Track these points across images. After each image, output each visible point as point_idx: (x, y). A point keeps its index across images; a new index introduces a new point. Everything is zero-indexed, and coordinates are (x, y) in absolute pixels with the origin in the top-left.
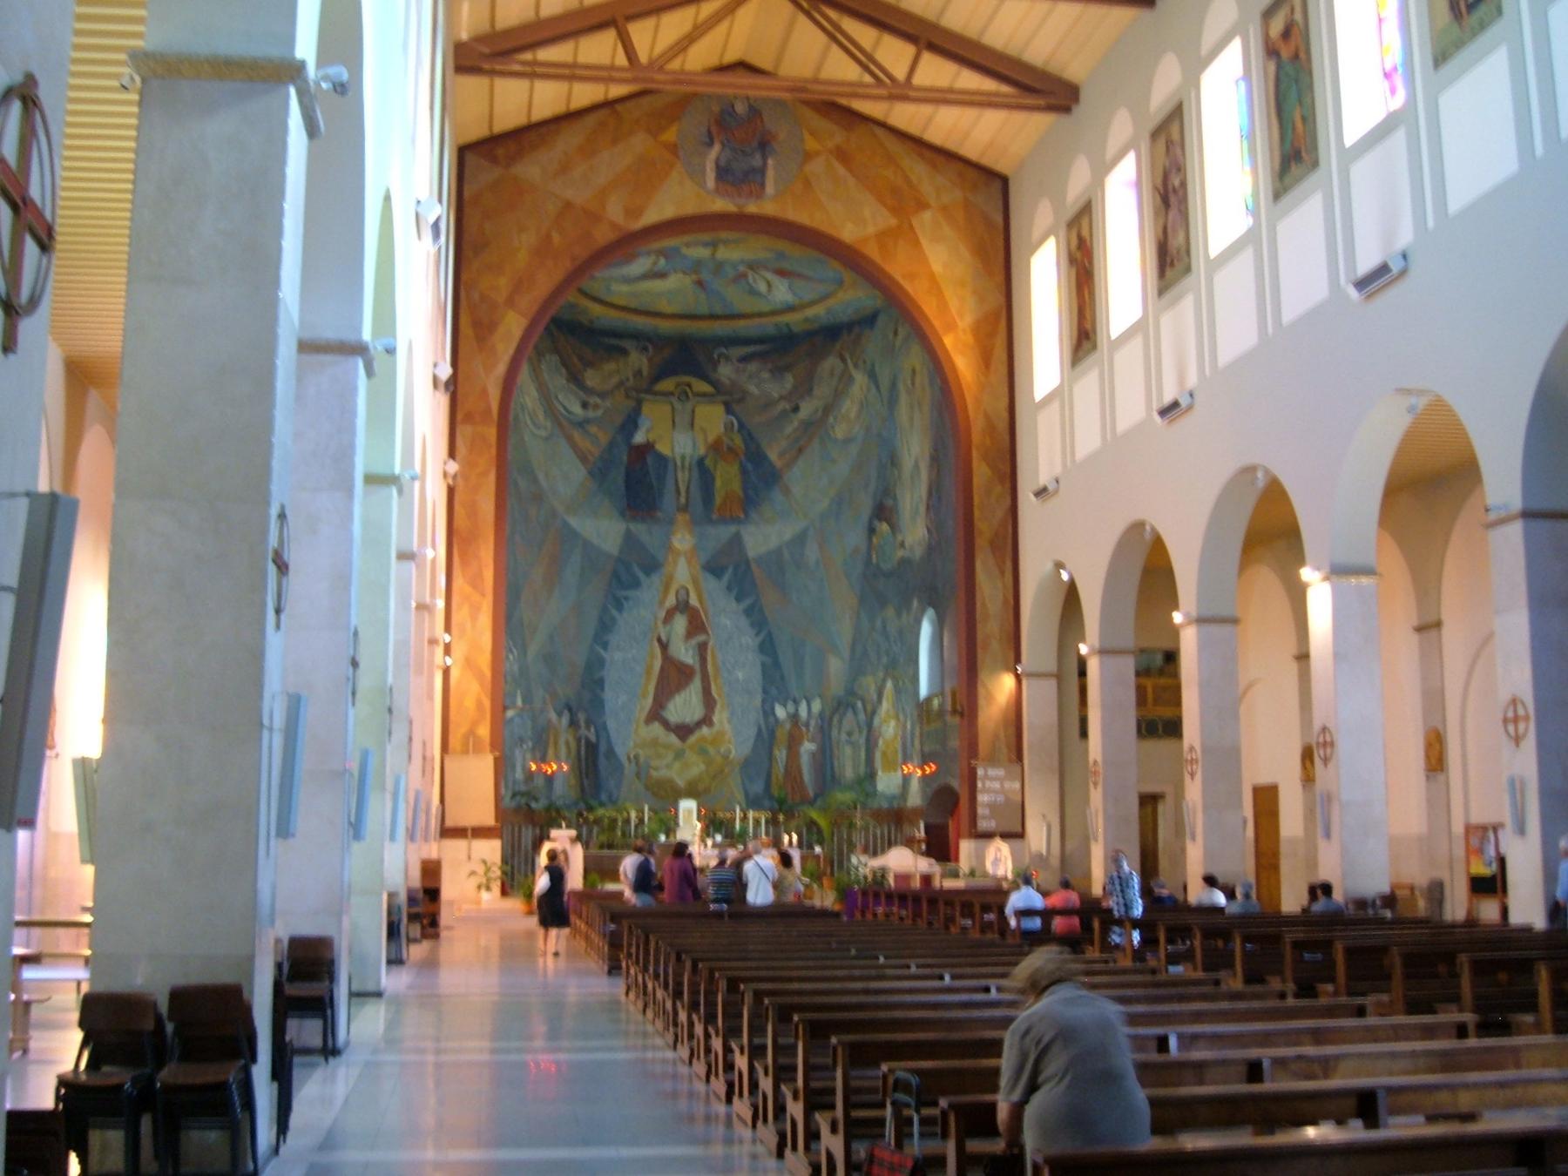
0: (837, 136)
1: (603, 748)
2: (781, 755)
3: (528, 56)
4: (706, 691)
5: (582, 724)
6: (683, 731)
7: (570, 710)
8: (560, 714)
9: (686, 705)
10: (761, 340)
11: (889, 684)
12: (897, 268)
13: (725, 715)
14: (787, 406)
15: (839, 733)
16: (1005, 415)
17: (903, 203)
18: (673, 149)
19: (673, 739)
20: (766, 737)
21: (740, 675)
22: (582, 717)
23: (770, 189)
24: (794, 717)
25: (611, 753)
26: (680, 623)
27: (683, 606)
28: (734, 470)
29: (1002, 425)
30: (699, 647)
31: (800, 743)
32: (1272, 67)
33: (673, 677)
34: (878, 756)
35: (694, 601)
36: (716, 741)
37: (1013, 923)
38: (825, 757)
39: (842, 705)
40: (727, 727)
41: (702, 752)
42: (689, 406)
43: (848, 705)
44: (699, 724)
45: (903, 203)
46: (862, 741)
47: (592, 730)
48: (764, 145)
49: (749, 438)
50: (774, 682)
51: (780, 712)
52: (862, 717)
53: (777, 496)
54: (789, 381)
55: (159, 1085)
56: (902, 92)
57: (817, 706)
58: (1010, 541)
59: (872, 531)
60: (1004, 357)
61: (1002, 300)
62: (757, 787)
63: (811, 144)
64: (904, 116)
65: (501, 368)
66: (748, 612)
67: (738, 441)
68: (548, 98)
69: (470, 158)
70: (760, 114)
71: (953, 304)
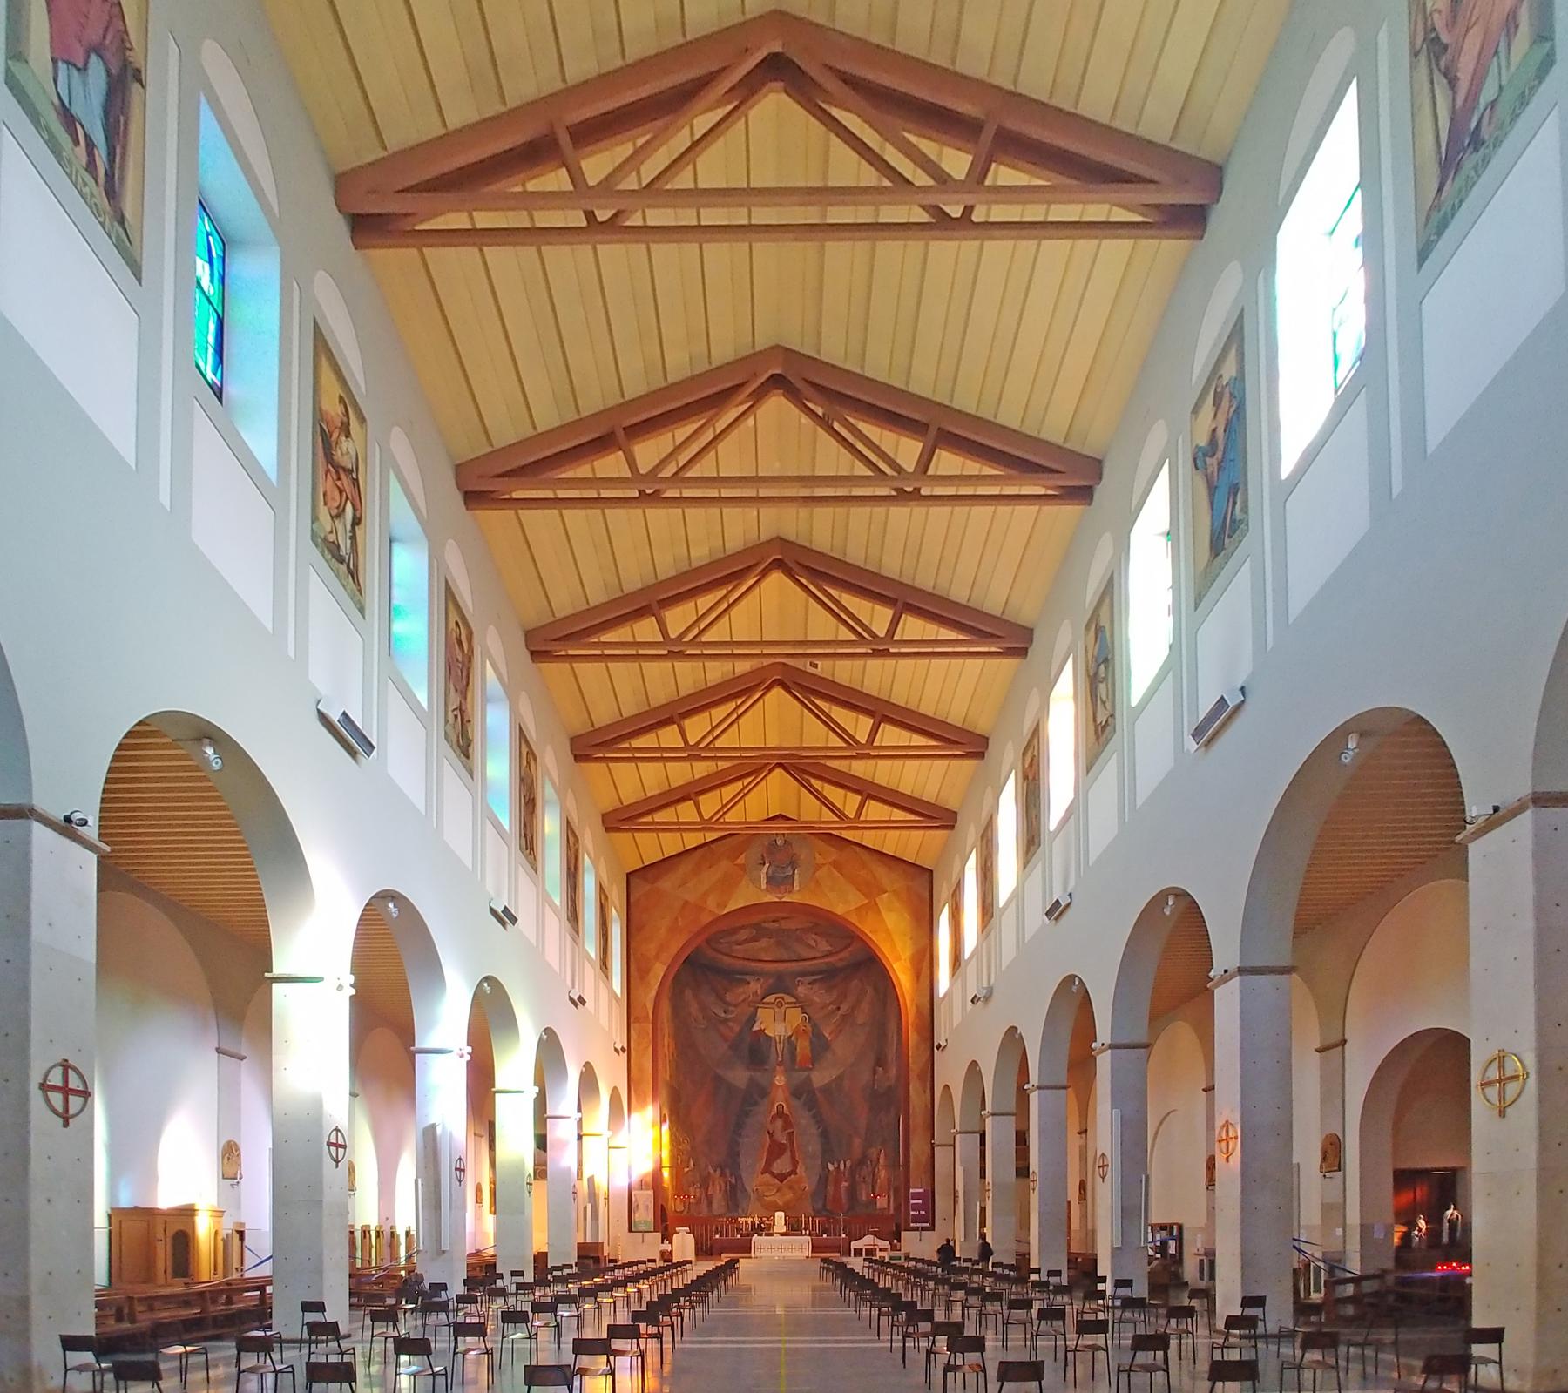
0: (833, 854)
1: (739, 1186)
2: (830, 1188)
3: (648, 819)
5: (728, 1175)
6: (782, 1178)
7: (721, 1167)
8: (715, 1171)
9: (781, 1165)
10: (820, 973)
12: (867, 927)
13: (803, 1169)
14: (834, 1007)
16: (929, 1006)
17: (871, 890)
18: (743, 867)
20: (824, 1180)
21: (810, 1149)
22: (727, 1171)
23: (796, 888)
26: (779, 1123)
27: (780, 1114)
28: (807, 1043)
29: (927, 1011)
31: (841, 1182)
32: (1025, 785)
33: (776, 1150)
35: (786, 1111)
37: (990, 1269)
38: (852, 1192)
39: (861, 1162)
40: (804, 1174)
41: (791, 1188)
42: (783, 1009)
44: (789, 1174)
45: (871, 890)
46: (870, 1181)
48: (793, 864)
49: (815, 1026)
50: (828, 1153)
51: (831, 1167)
53: (829, 1055)
54: (835, 995)
56: (857, 823)
58: (929, 1075)
59: (875, 1073)
60: (928, 972)
61: (928, 942)
62: (819, 1205)
63: (819, 860)
64: (869, 839)
65: (654, 993)
66: (814, 1116)
67: (809, 1028)
68: (671, 844)
69: (632, 880)
70: (791, 844)
71: (899, 945)
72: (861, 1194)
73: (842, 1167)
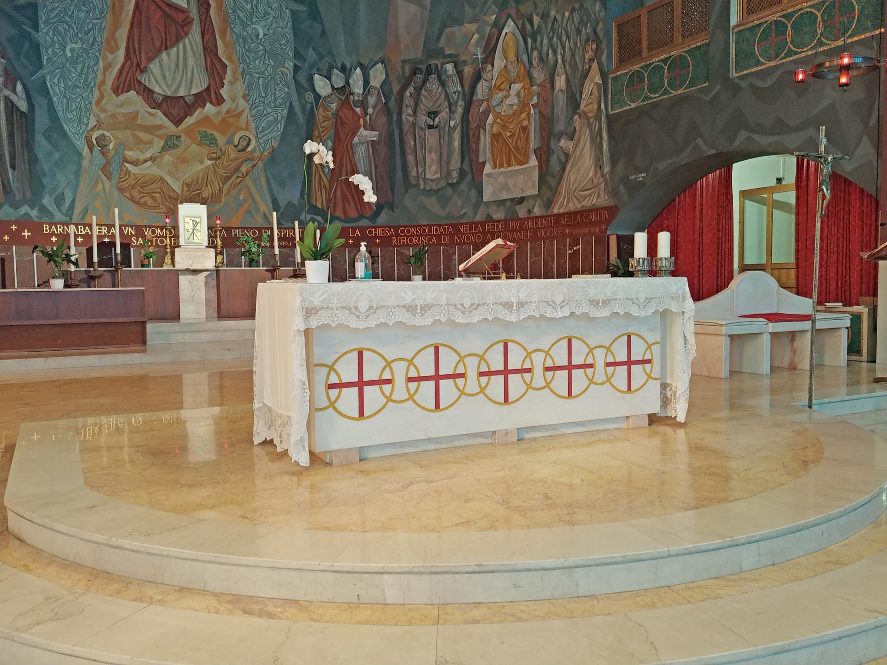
1: (41, 121)
4: (210, 50)
11: (510, 27)
15: (415, 113)
19: (160, 118)
24: (344, 91)
25: (56, 129)
30: (205, 117)
31: (354, 133)
34: (485, 140)
36: (227, 124)
40: (243, 105)
43: (429, 72)
44: (200, 99)
47: (19, 87)
51: (322, 86)
52: (455, 87)
55: (765, 196)
57: (378, 76)
62: (291, 195)
72: (421, 162)
73: (357, 87)
